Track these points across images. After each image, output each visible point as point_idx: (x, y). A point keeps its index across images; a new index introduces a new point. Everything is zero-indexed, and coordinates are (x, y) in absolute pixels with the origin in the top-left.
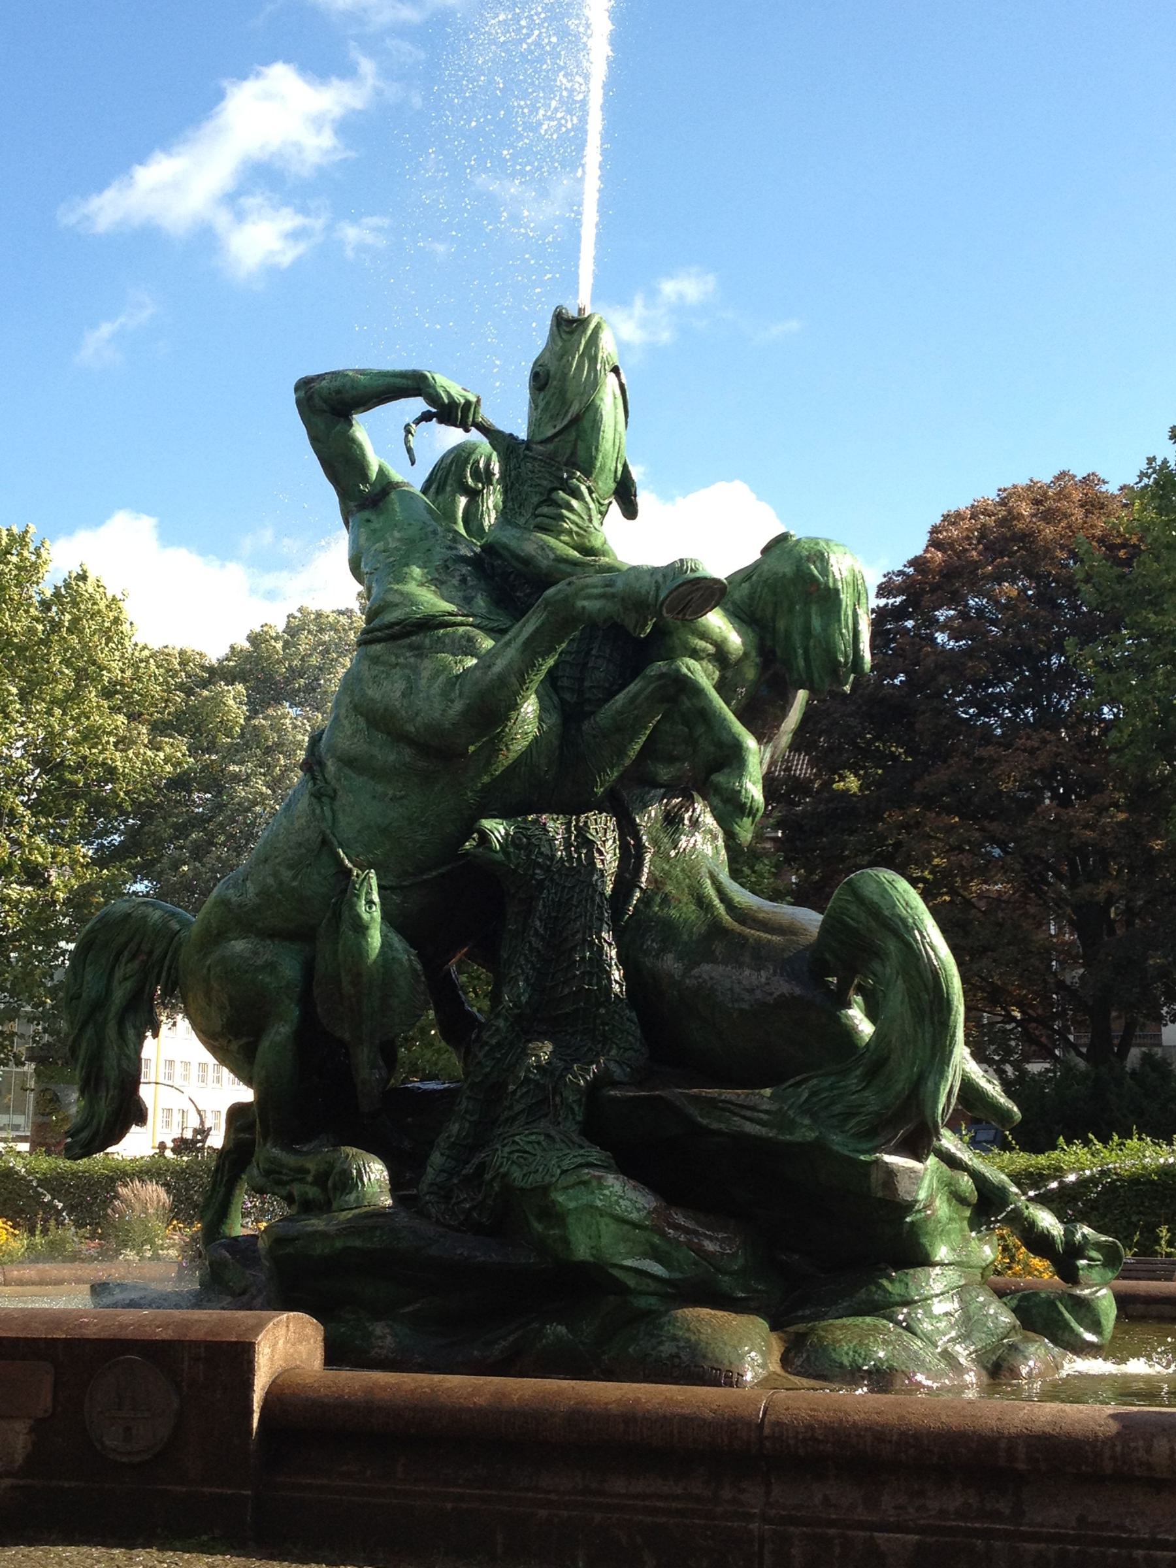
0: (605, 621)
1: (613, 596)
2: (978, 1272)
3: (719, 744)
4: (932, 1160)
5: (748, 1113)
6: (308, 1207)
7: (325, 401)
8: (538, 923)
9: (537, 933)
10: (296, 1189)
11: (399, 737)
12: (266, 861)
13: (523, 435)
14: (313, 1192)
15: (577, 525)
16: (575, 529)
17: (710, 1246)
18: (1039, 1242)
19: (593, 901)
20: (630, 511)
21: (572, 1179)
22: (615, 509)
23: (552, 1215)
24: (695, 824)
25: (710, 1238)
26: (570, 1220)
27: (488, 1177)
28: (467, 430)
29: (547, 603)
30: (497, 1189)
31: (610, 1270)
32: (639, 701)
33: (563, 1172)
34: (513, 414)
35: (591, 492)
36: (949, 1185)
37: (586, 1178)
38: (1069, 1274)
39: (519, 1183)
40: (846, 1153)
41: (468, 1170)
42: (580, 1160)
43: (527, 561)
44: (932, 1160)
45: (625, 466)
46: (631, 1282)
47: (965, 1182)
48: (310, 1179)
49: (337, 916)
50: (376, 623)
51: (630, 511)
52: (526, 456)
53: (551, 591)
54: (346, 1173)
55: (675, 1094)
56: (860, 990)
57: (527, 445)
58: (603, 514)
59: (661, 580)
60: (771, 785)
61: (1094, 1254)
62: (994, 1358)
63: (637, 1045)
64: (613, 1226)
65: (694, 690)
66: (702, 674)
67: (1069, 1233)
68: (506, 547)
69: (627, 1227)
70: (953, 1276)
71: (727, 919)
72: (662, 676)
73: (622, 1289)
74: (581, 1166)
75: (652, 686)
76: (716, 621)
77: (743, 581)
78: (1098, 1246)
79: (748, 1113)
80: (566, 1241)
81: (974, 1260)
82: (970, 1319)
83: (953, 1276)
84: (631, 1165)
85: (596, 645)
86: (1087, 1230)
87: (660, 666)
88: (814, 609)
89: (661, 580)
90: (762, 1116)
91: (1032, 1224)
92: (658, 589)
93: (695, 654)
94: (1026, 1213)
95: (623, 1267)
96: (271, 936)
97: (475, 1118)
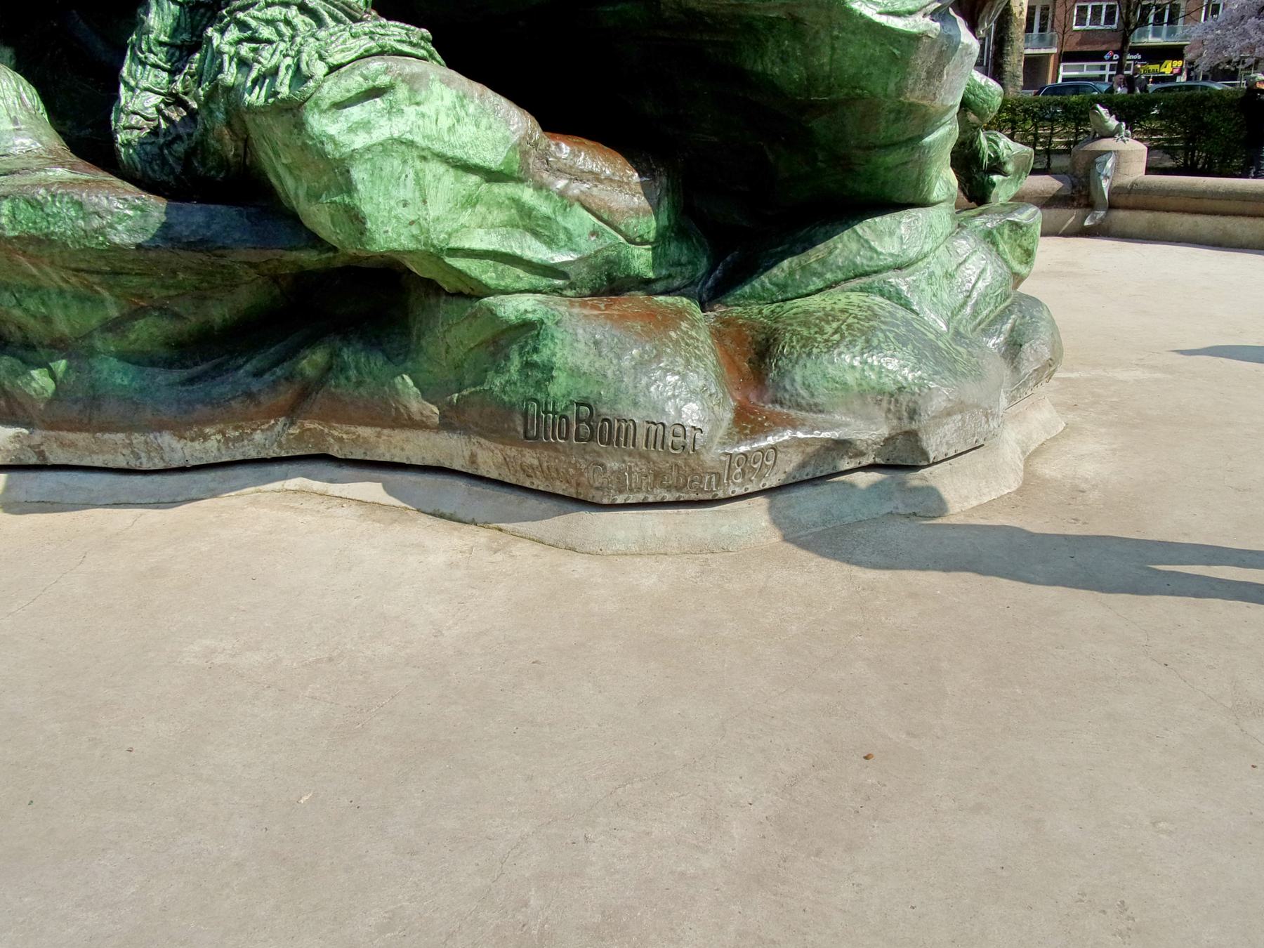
21: (353, 83)
23: (336, 172)
26: (359, 174)
33: (333, 69)
37: (383, 80)
42: (365, 43)
46: (486, 273)
69: (474, 179)
73: (472, 292)
80: (355, 218)
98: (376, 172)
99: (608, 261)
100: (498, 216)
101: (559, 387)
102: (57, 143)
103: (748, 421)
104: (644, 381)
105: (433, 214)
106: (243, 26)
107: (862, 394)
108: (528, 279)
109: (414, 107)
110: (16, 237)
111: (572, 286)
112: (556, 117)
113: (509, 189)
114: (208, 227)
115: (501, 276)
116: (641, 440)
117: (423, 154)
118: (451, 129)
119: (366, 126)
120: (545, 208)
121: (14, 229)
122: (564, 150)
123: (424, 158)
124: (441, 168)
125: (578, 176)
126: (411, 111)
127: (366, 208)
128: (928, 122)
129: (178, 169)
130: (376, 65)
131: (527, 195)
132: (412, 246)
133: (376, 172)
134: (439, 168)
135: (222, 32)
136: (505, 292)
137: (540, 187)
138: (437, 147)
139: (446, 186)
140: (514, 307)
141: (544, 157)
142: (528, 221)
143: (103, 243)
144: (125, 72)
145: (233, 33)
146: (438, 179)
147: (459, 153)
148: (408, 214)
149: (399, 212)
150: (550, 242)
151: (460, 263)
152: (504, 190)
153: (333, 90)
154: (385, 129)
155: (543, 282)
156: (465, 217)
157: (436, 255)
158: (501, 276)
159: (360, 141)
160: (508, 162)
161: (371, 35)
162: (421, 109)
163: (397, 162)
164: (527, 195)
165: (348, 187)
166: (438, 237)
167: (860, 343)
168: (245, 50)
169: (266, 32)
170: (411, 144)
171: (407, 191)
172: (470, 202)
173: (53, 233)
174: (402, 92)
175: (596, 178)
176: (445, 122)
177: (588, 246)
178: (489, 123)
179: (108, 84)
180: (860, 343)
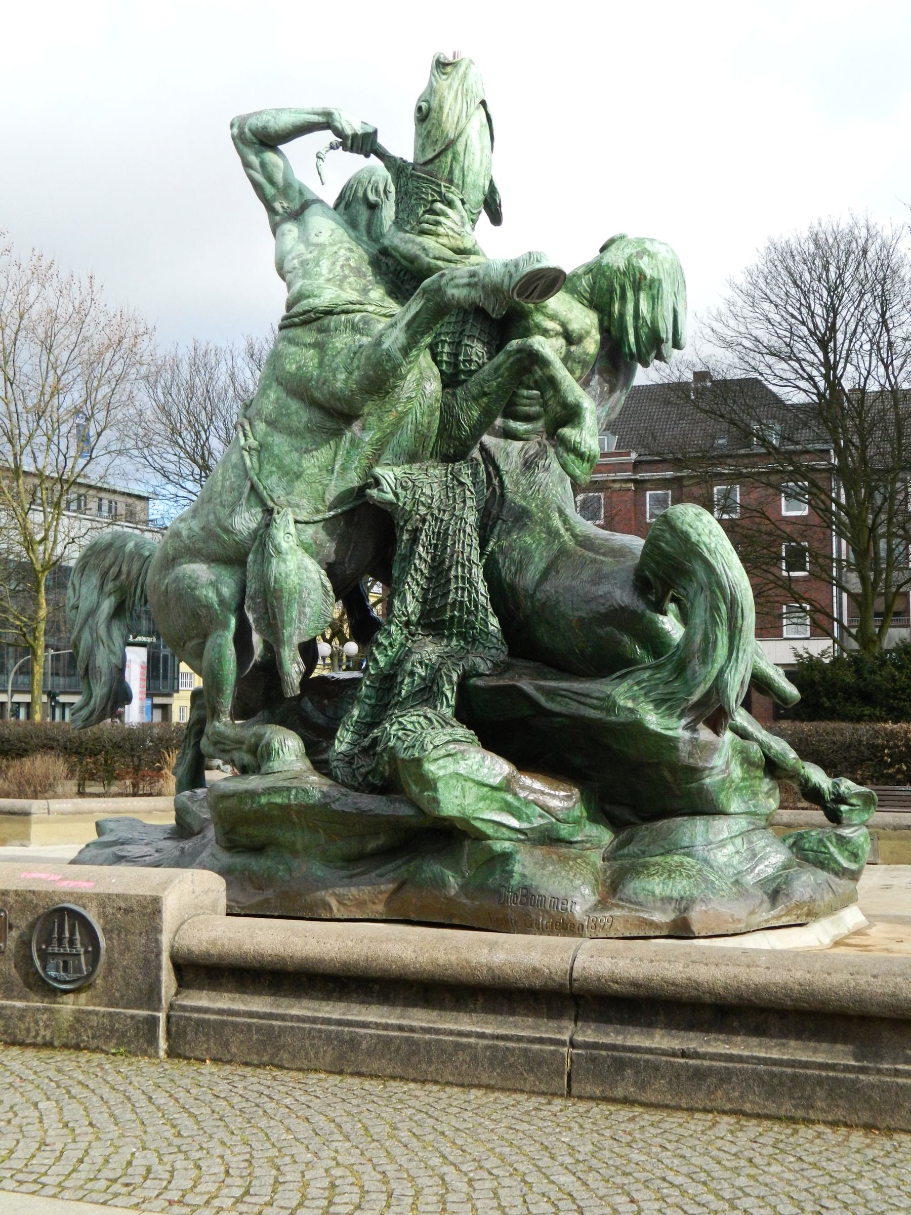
0: (471, 305)
1: (476, 284)
2: (763, 818)
3: (565, 405)
4: (728, 735)
5: (583, 699)
6: (245, 770)
7: (254, 135)
8: (421, 549)
9: (420, 557)
10: (236, 755)
11: (313, 403)
12: (209, 501)
13: (410, 159)
14: (247, 758)
15: (453, 230)
16: (451, 233)
17: (554, 803)
18: (813, 795)
19: (464, 532)
20: (496, 218)
21: (442, 752)
22: (484, 217)
23: (429, 784)
24: (547, 469)
25: (554, 796)
26: (440, 785)
27: (379, 749)
28: (367, 156)
29: (425, 291)
30: (386, 758)
31: (473, 822)
32: (502, 370)
33: (435, 747)
34: (402, 142)
35: (463, 203)
36: (741, 752)
37: (453, 751)
38: (835, 818)
39: (402, 755)
40: (659, 730)
41: (366, 742)
42: (448, 738)
43: (412, 259)
44: (728, 735)
45: (491, 181)
46: (489, 830)
47: (755, 748)
48: (245, 747)
49: (263, 545)
50: (295, 310)
51: (496, 218)
52: (412, 175)
53: (427, 282)
54: (268, 745)
55: (526, 685)
56: (674, 600)
57: (414, 166)
58: (474, 221)
59: (513, 269)
60: (233, 830)
61: (854, 801)
62: (774, 885)
63: (499, 645)
64: (475, 789)
65: (544, 362)
66: (549, 348)
67: (836, 785)
68: (396, 249)
69: (486, 789)
70: (742, 823)
71: (571, 544)
72: (519, 350)
73: (481, 837)
74: (449, 742)
75: (512, 359)
76: (560, 303)
77: (586, 273)
78: (858, 795)
79: (583, 699)
80: (436, 801)
81: (761, 810)
82: (755, 855)
83: (742, 823)
84: (492, 741)
85: (468, 326)
86: (850, 783)
87: (515, 343)
88: (642, 295)
89: (513, 269)
90: (595, 702)
91: (807, 780)
92: (511, 276)
93: (545, 332)
94: (802, 771)
95: (483, 820)
96: (213, 561)
97: (373, 701)
98: (447, 784)
99: (547, 830)
100: (496, 805)
101: (515, 880)
102: (311, 767)
103: (602, 904)
105: (467, 802)
106: (400, 723)
107: (662, 899)
108: (508, 833)
111: (529, 840)
112: (524, 761)
113: (502, 794)
115: (496, 832)
116: (548, 905)
118: (477, 770)
119: (445, 767)
120: (516, 803)
122: (526, 780)
124: (472, 784)
125: (534, 791)
127: (441, 798)
129: (360, 779)
130: (451, 746)
131: (509, 798)
132: (458, 815)
133: (447, 784)
135: (392, 725)
136: (497, 839)
137: (515, 794)
138: (471, 776)
139: (473, 791)
140: (499, 846)
141: (518, 782)
142: (509, 809)
144: (338, 734)
146: (470, 788)
147: (479, 779)
148: (457, 801)
149: (453, 802)
150: (519, 818)
151: (478, 824)
152: (497, 794)
153: (434, 755)
155: (514, 836)
156: (481, 804)
157: (465, 820)
158: (496, 832)
159: (441, 773)
160: (500, 783)
161: (450, 735)
164: (509, 798)
165: (435, 789)
166: (469, 812)
167: (666, 875)
168: (400, 733)
169: (409, 727)
171: (458, 793)
172: (483, 798)
174: (459, 756)
175: (543, 793)
176: (475, 767)
177: (537, 822)
178: (497, 768)
179: (330, 735)
180: (666, 875)
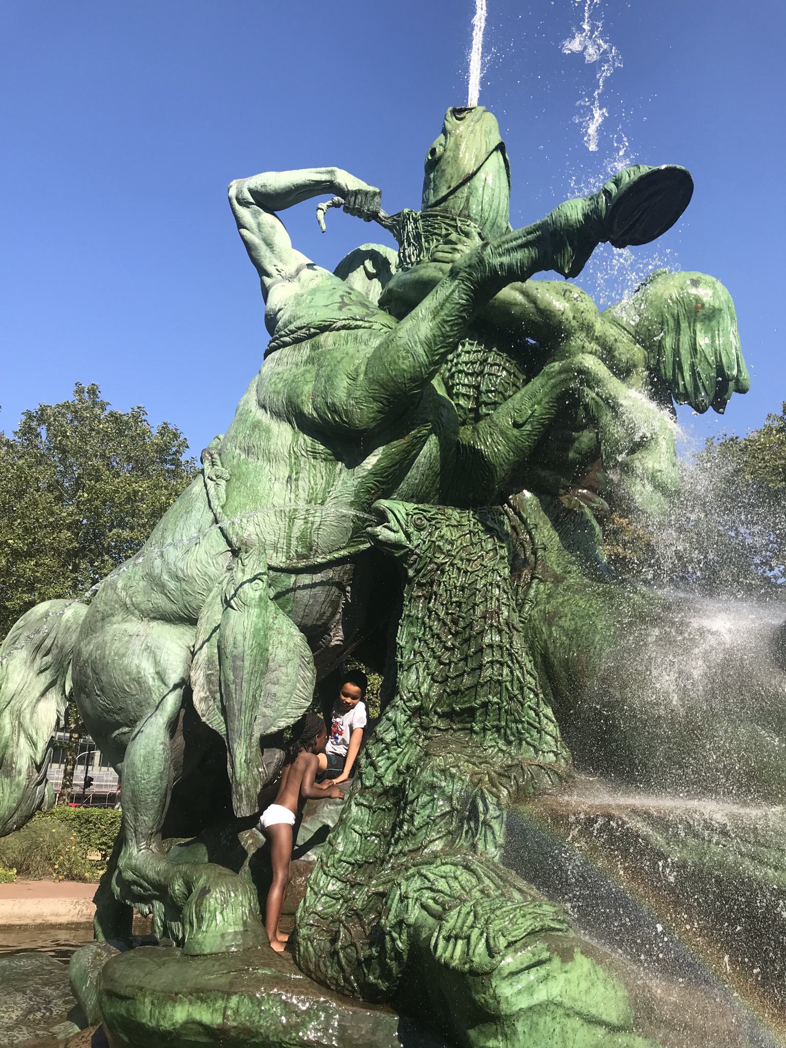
69: (601, 1032)
98: (534, 1027)
104: (491, 991)
109: (565, 975)
110: (234, 1027)
114: (373, 1034)
117: (568, 1012)
118: (587, 991)
121: (234, 1020)
123: (568, 1015)
126: (562, 977)
128: (589, 17)
134: (576, 1022)
143: (294, 1039)
145: (417, 883)
146: (574, 1031)
153: (510, 962)
154: (541, 995)
162: (568, 975)
163: (548, 1019)
170: (559, 1005)
173: (261, 1026)
